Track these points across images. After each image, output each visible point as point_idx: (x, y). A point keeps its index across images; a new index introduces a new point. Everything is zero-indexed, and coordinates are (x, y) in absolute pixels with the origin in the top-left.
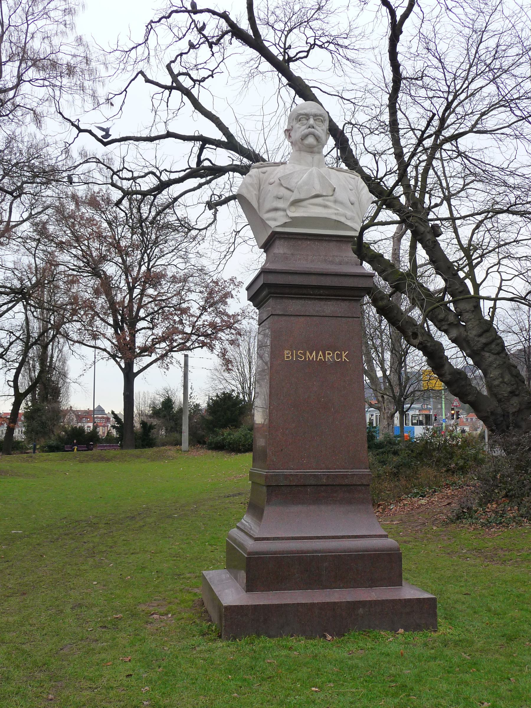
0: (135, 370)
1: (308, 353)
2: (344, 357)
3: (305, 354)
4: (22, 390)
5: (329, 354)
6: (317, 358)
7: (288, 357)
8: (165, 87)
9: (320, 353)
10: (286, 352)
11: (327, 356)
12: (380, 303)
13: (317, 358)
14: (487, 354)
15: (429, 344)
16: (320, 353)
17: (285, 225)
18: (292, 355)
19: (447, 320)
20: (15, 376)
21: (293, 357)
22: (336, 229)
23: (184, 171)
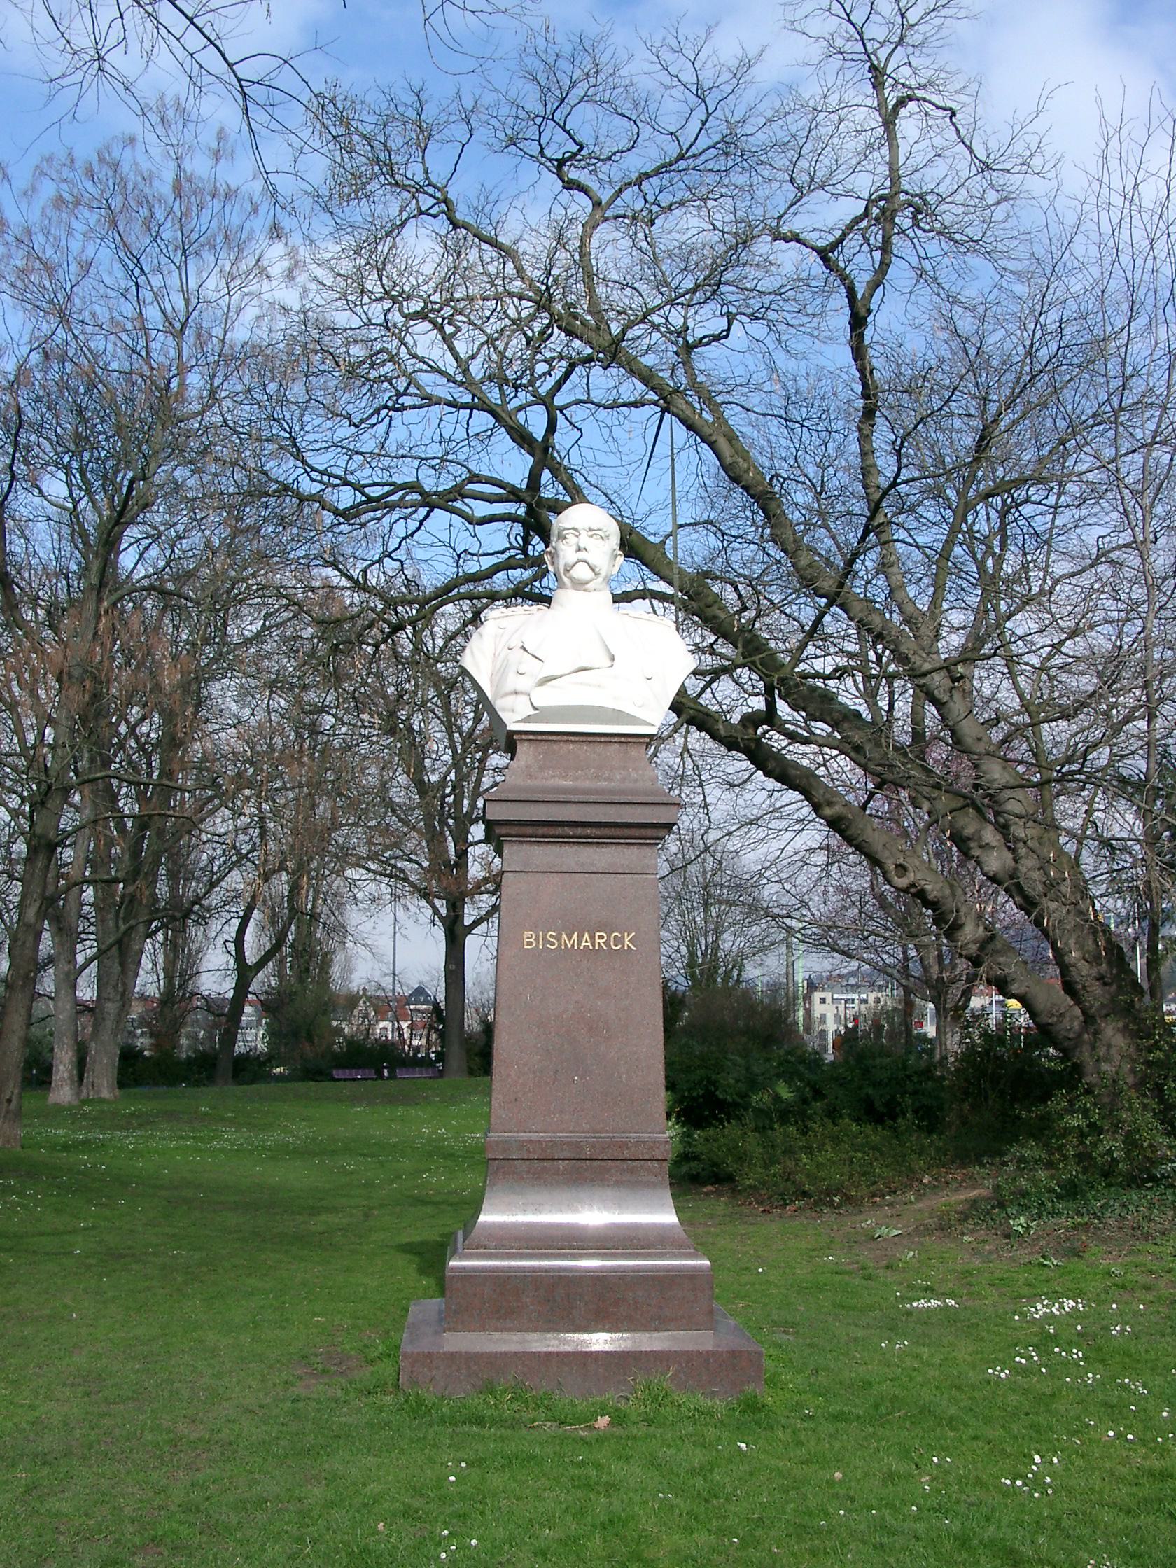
0: (468, 921)
1: (565, 937)
2: (627, 942)
3: (559, 938)
4: (251, 957)
5: (601, 937)
6: (579, 944)
7: (530, 943)
8: (464, 406)
9: (586, 935)
10: (527, 934)
11: (597, 940)
12: (828, 811)
13: (579, 944)
14: (1053, 905)
15: (928, 887)
16: (586, 935)
17: (528, 720)
18: (537, 939)
19: (980, 838)
20: (237, 932)
21: (538, 943)
22: (618, 722)
23: (503, 552)
